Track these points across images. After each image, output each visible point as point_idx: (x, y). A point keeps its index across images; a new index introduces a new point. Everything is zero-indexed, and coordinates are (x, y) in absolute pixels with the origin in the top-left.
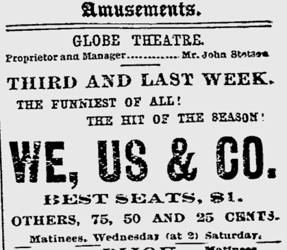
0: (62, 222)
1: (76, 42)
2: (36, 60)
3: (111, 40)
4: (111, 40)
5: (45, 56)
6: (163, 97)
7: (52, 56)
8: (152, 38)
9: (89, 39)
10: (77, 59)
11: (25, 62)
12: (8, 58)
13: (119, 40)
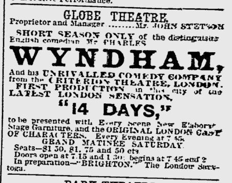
0: (65, 89)
1: (66, 14)
2: (33, 24)
3: (94, 16)
4: (94, 16)
5: (41, 21)
6: (96, 72)
7: (46, 21)
8: (127, 15)
9: (77, 14)
10: (66, 25)
11: (25, 25)
12: (12, 21)
13: (100, 16)
